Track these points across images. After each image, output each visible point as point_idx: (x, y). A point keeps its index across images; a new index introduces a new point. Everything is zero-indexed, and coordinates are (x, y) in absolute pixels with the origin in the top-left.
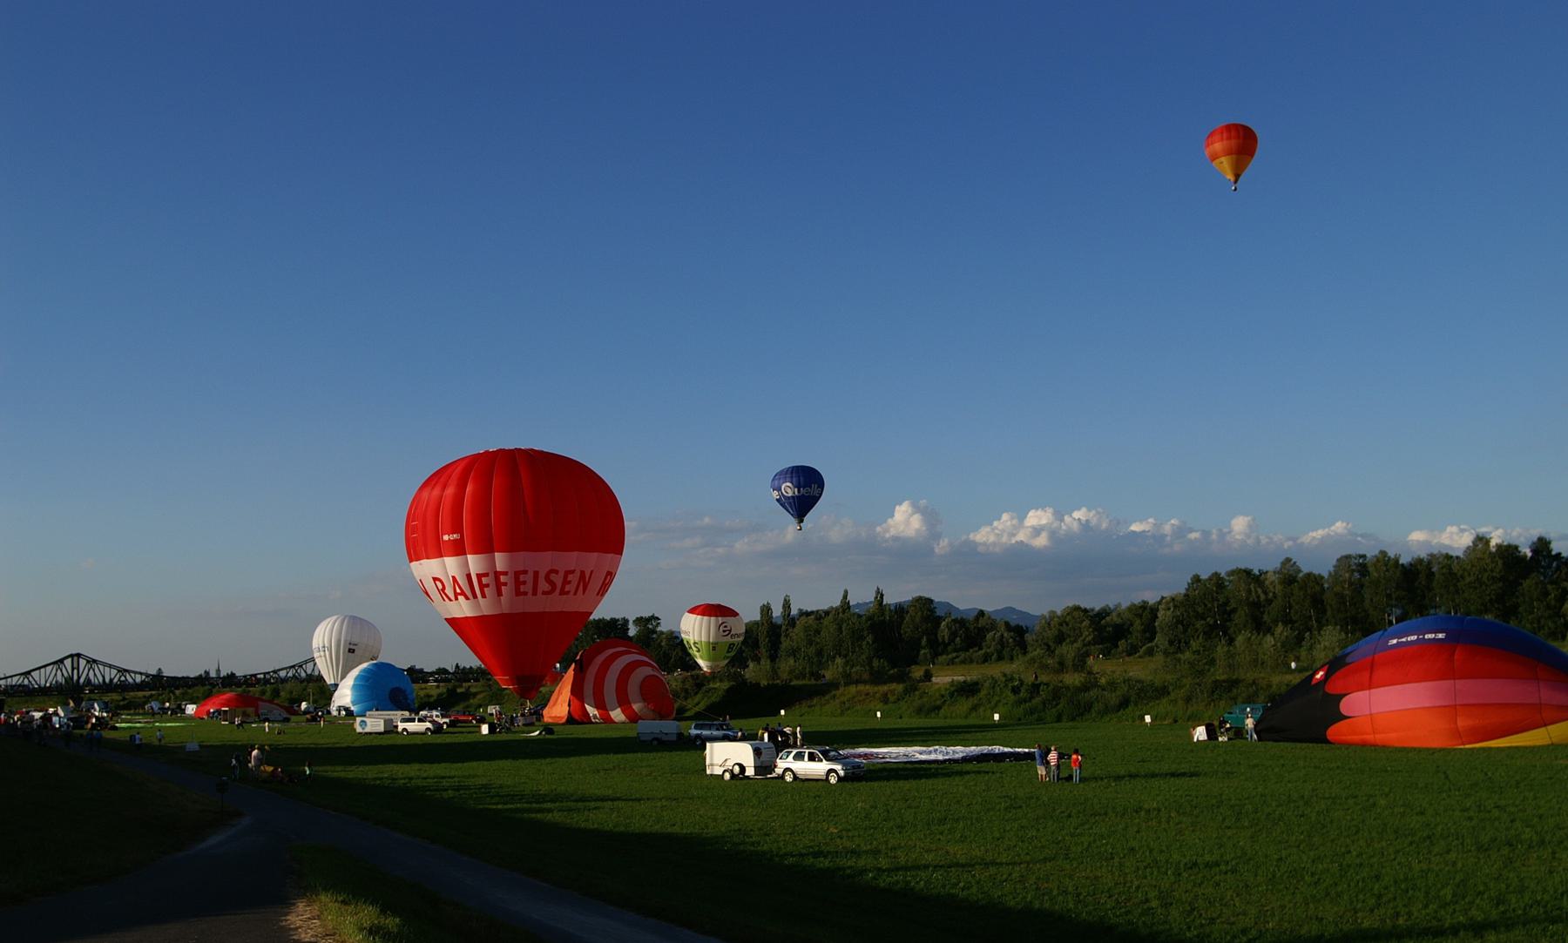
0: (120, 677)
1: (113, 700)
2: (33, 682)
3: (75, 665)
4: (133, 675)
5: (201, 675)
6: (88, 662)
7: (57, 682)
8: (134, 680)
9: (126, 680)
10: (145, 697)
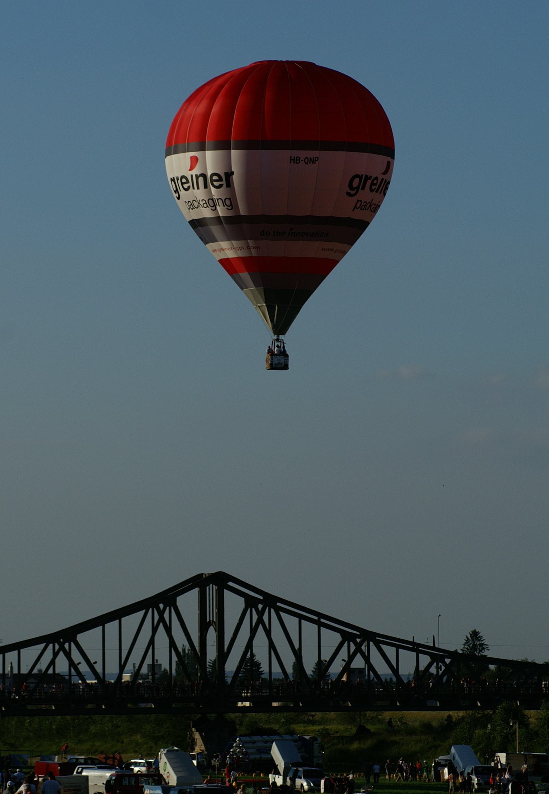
0: (351, 658)
1: (325, 734)
2: (84, 668)
3: (212, 614)
4: (390, 651)
5: (456, 651)
6: (250, 603)
7: (154, 667)
8: (395, 671)
9: (371, 668)
10: (427, 727)
